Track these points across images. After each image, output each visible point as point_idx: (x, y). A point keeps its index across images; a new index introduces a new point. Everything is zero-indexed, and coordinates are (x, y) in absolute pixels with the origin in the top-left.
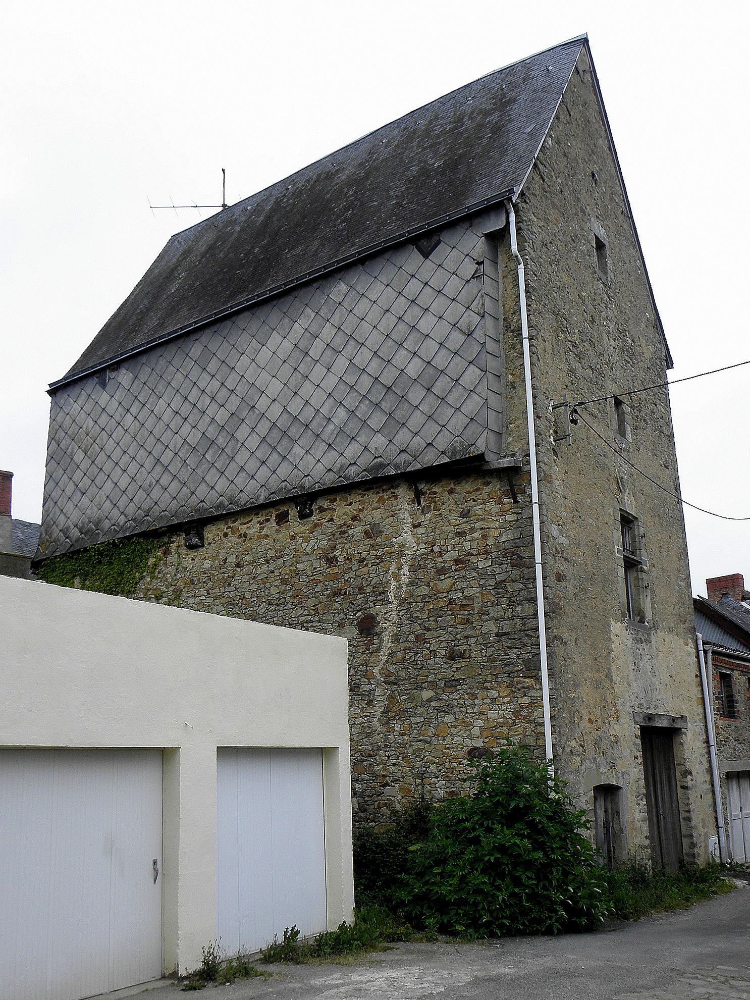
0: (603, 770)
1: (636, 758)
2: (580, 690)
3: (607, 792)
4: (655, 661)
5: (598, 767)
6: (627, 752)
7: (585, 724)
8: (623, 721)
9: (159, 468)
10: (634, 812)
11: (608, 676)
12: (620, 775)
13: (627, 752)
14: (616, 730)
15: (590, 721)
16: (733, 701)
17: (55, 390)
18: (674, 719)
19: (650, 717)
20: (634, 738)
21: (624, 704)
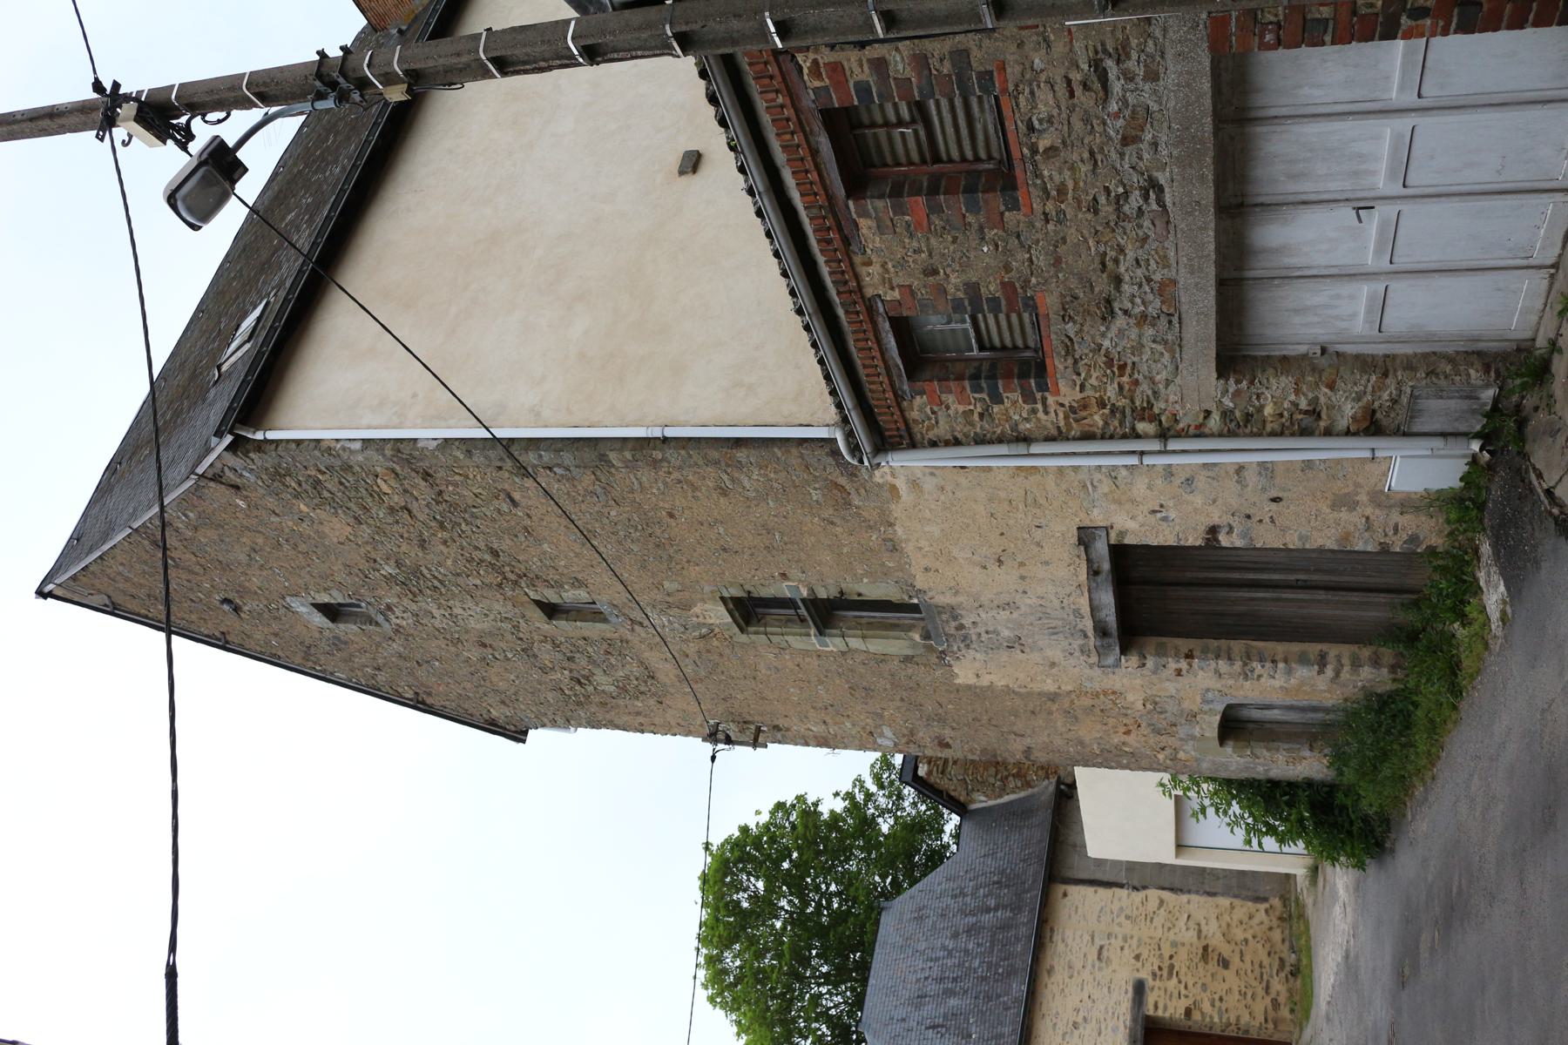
0: (1197, 731)
1: (1179, 673)
2: (1087, 740)
3: (1233, 726)
4: (984, 599)
5: (1193, 737)
6: (1170, 688)
7: (1131, 739)
8: (1117, 687)
9: (893, 119)
10: (1280, 683)
11: (1053, 697)
12: (1206, 708)
13: (1170, 688)
14: (1135, 699)
15: (1128, 733)
16: (971, 190)
17: (519, 736)
18: (1094, 572)
19: (1101, 631)
20: (1145, 671)
21: (1091, 679)
